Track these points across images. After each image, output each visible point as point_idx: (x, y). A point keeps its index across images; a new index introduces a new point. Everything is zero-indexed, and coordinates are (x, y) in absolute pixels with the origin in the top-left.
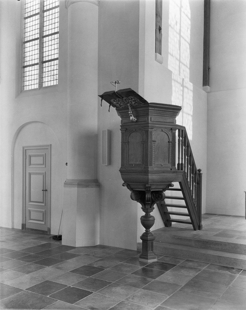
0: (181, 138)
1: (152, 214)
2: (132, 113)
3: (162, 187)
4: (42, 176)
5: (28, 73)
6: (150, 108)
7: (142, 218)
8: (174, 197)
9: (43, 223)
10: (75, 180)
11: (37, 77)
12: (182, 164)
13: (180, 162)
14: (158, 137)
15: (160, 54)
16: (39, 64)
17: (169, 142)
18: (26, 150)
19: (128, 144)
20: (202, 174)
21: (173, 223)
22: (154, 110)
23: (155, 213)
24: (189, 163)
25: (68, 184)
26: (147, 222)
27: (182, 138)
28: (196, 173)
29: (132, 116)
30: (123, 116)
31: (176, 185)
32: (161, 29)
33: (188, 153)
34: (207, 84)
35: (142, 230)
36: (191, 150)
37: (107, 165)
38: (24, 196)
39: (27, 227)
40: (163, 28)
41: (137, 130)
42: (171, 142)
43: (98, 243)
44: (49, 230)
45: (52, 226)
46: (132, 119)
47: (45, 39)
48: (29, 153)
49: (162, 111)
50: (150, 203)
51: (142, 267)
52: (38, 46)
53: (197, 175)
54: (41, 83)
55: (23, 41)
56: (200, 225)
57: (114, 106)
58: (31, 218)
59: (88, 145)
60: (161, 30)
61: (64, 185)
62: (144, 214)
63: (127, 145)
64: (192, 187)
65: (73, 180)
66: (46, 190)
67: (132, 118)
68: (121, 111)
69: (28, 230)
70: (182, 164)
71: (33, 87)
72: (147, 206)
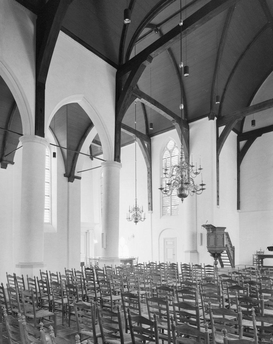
1: (217, 261)
8: (224, 256)
14: (220, 237)
23: (218, 260)
31: (225, 252)
40: (219, 196)
53: (233, 249)
62: (215, 261)
64: (231, 252)
67: (211, 232)
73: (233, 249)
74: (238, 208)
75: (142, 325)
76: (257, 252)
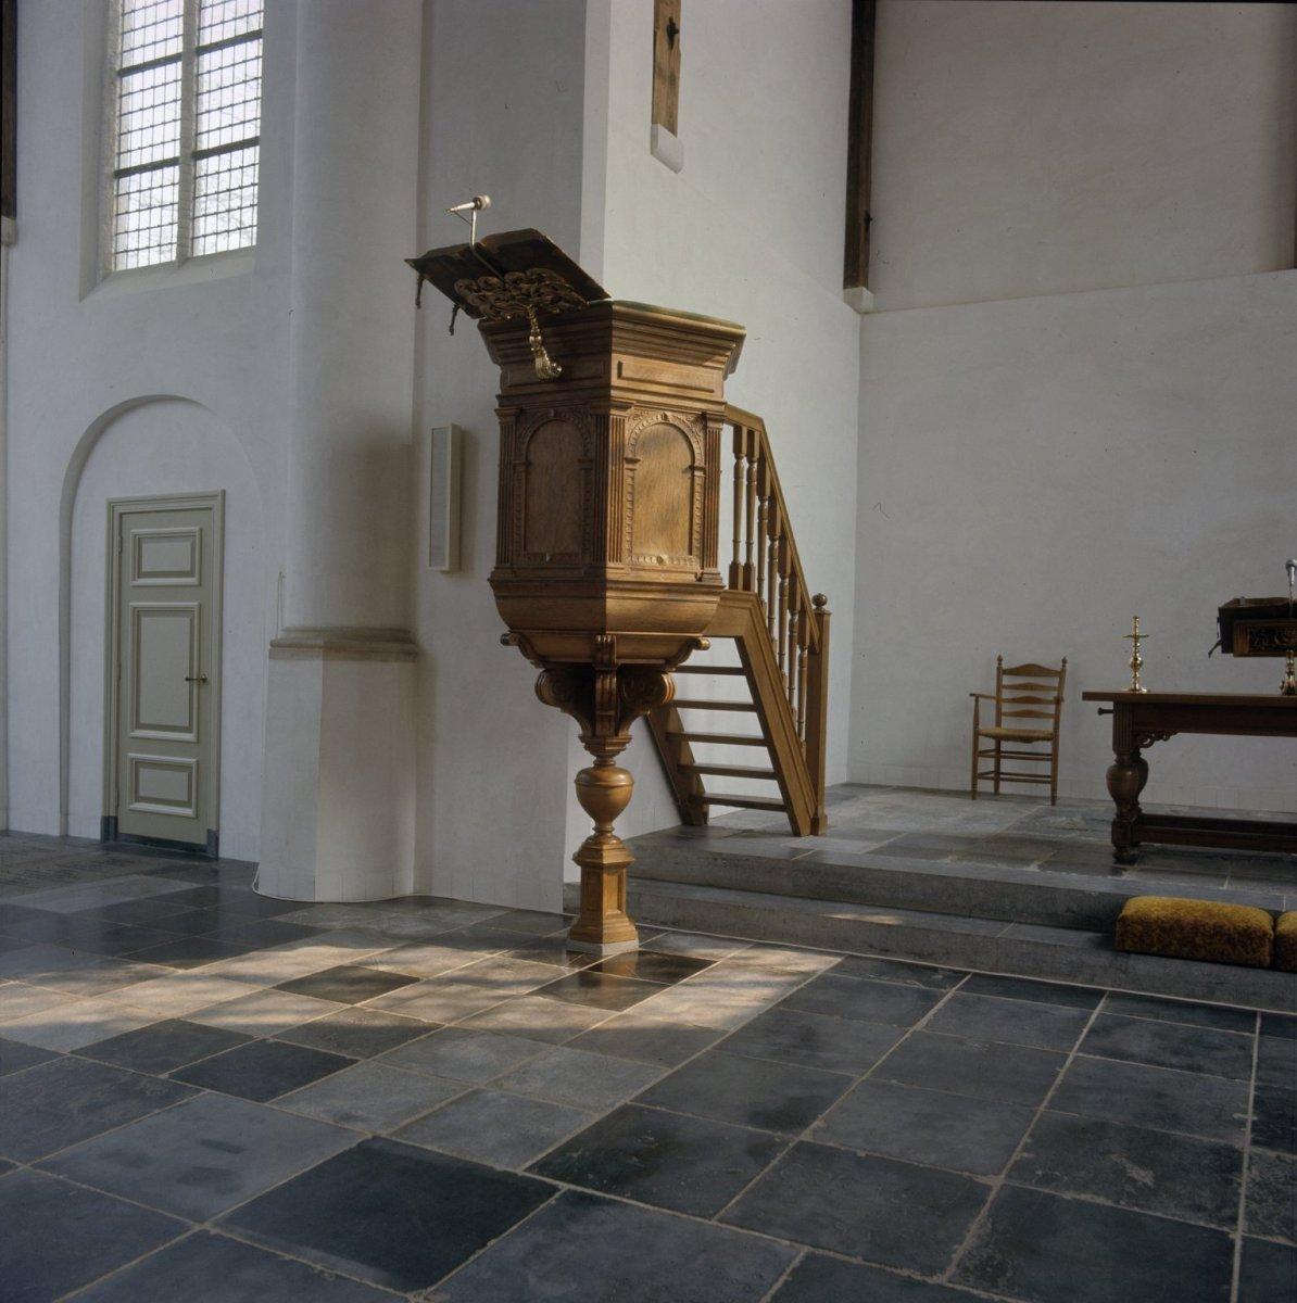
0: (745, 463)
2: (543, 343)
3: (661, 650)
4: (188, 620)
5: (137, 98)
6: (615, 323)
7: (583, 776)
8: (710, 692)
9: (189, 812)
10: (314, 630)
11: (174, 111)
12: (748, 566)
13: (742, 560)
15: (673, 129)
16: (180, 161)
17: (692, 468)
18: (121, 515)
19: (527, 472)
20: (829, 614)
21: (715, 811)
22: (633, 332)
23: (635, 764)
24: (776, 569)
25: (286, 648)
26: (599, 800)
27: (750, 462)
28: (803, 612)
29: (542, 355)
30: (506, 356)
31: (723, 651)
32: (677, 31)
33: (774, 525)
34: (861, 278)
35: (580, 826)
36: (796, 553)
37: (446, 567)
38: (115, 585)
39: (124, 828)
41: (563, 415)
42: (700, 469)
43: (408, 887)
44: (214, 837)
45: (223, 823)
46: (544, 366)
47: (208, 61)
48: (135, 529)
49: (665, 338)
50: (612, 713)
51: (577, 970)
52: (179, 90)
53: (810, 621)
54: (186, 238)
55: (118, 68)
56: (816, 814)
57: (472, 311)
58: (142, 794)
59: (373, 478)
60: (676, 35)
61: (270, 651)
62: (589, 760)
63: (523, 474)
65: (304, 630)
66: (204, 680)
67: (544, 362)
68: (496, 337)
69: (126, 840)
70: (748, 566)
71: (155, 258)
72: (600, 743)
73: (810, 623)
74: (857, 267)
75: (754, 699)
76: (1001, 672)
